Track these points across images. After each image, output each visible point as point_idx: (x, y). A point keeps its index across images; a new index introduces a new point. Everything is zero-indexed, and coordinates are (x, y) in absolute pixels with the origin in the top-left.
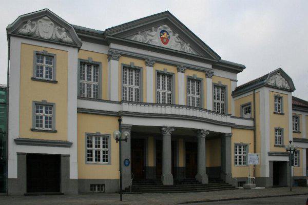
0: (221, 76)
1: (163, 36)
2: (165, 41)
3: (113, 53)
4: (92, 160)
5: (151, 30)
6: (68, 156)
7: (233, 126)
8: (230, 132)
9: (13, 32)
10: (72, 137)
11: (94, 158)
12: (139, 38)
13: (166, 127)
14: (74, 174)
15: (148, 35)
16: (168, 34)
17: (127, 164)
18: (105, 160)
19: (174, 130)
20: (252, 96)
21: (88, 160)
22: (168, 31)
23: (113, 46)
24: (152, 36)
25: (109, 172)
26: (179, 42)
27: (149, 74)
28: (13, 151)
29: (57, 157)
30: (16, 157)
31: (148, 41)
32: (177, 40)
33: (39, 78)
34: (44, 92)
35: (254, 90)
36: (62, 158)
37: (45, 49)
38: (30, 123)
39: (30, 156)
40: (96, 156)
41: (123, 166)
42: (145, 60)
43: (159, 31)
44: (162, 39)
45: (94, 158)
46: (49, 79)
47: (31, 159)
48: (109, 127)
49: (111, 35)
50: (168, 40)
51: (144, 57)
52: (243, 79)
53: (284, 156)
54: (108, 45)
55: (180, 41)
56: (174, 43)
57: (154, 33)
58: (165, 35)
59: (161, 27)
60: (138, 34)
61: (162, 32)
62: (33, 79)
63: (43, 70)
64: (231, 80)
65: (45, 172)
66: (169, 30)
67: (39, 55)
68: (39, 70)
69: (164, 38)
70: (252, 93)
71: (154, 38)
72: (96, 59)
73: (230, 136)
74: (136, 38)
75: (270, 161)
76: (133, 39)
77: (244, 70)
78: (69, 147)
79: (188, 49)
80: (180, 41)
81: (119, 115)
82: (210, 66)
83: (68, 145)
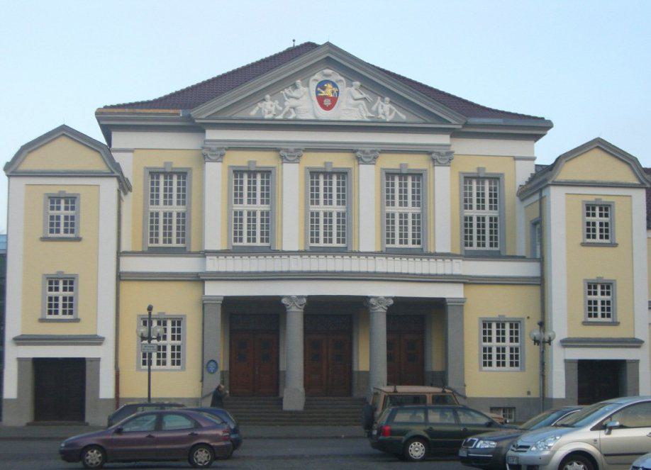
0: (479, 153)
1: (323, 93)
2: (327, 102)
3: (210, 149)
4: (490, 364)
5: (295, 87)
6: (98, 360)
7: (467, 281)
8: (461, 296)
9: (12, 170)
10: (105, 328)
11: (494, 360)
12: (268, 108)
13: (289, 297)
14: (106, 391)
15: (289, 97)
16: (334, 85)
17: (212, 369)
18: (177, 362)
19: (305, 300)
20: (538, 204)
21: (485, 364)
22: (334, 80)
23: (211, 135)
24: (297, 98)
25: (180, 383)
26: (365, 99)
27: (291, 180)
28: (13, 353)
29: (81, 362)
30: (562, 365)
31: (287, 109)
32: (358, 96)
33: (55, 235)
34: (62, 258)
35: (541, 190)
36: (88, 363)
37: (62, 189)
38: (39, 307)
39: (38, 363)
40: (498, 357)
41: (206, 374)
42: (279, 151)
43: (313, 85)
44: (321, 100)
45: (494, 360)
46: (69, 235)
47: (40, 366)
48: (176, 301)
49: (203, 116)
50: (334, 100)
51: (275, 146)
52: (545, 151)
53: (626, 347)
54: (204, 132)
55: (365, 95)
56: (352, 104)
57: (302, 89)
58: (329, 91)
59: (319, 77)
60: (264, 100)
61: (321, 85)
62: (44, 239)
63: (62, 220)
64: (515, 159)
65: (59, 385)
66: (336, 77)
67: (54, 200)
68: (54, 224)
69: (326, 97)
70: (537, 197)
71: (302, 102)
72: (179, 163)
73: (460, 304)
74: (260, 109)
75: (567, 362)
76: (253, 113)
77: (550, 132)
78: (100, 344)
79: (386, 110)
80: (365, 95)
81: (199, 279)
82: (444, 139)
83: (96, 340)
